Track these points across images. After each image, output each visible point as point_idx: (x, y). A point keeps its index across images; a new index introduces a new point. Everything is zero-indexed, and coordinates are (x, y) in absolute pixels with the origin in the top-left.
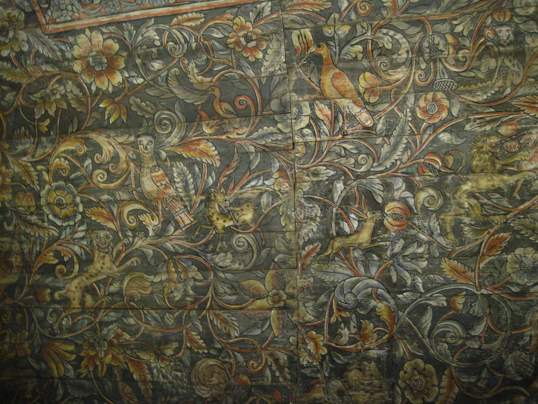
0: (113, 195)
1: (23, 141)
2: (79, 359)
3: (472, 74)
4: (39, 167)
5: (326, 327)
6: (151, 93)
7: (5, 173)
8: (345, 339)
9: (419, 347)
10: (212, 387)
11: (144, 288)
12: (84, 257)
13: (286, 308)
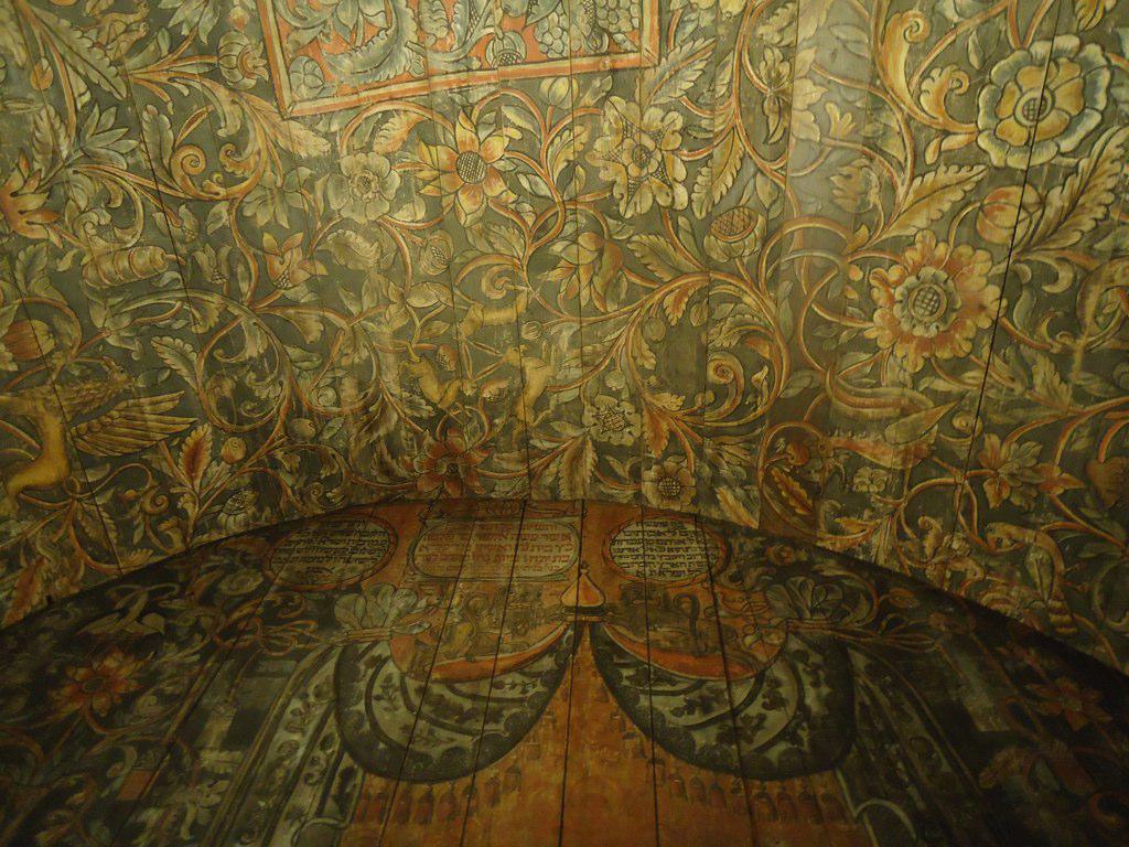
4: (930, 157)
7: (923, 257)
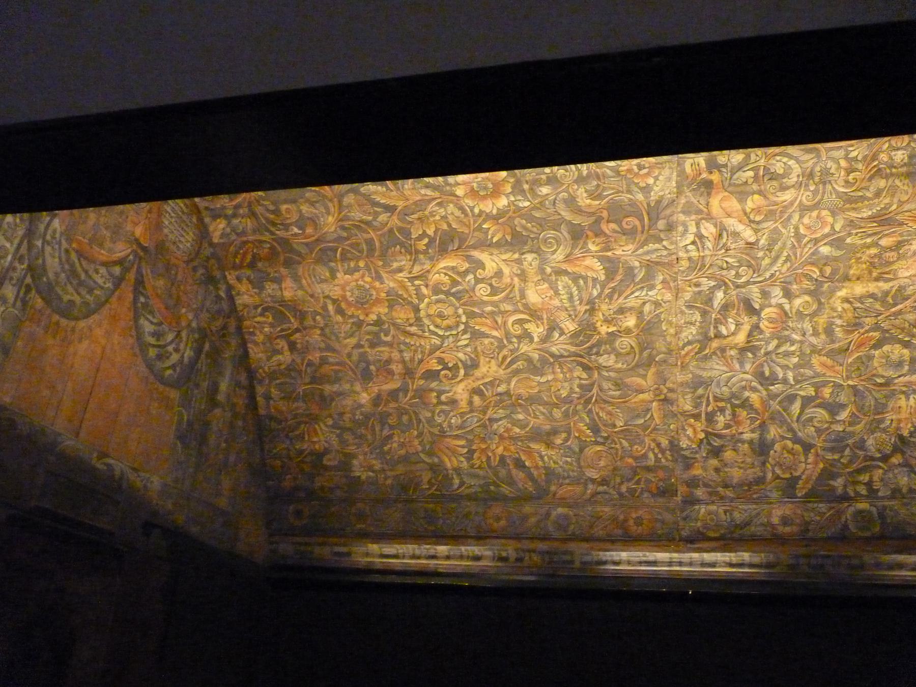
0: (497, 306)
1: (398, 258)
2: (471, 452)
3: (860, 194)
4: (417, 282)
5: (703, 416)
6: (537, 215)
8: (720, 425)
9: (788, 430)
10: (600, 469)
11: (531, 387)
12: (469, 363)
13: (666, 400)
